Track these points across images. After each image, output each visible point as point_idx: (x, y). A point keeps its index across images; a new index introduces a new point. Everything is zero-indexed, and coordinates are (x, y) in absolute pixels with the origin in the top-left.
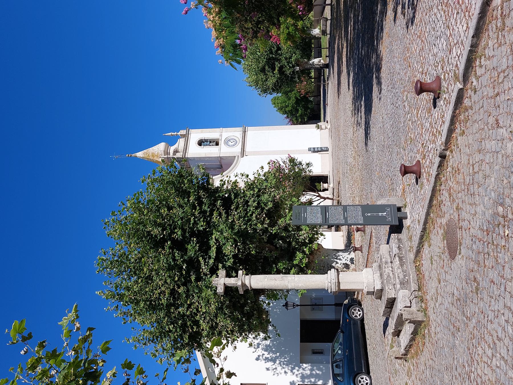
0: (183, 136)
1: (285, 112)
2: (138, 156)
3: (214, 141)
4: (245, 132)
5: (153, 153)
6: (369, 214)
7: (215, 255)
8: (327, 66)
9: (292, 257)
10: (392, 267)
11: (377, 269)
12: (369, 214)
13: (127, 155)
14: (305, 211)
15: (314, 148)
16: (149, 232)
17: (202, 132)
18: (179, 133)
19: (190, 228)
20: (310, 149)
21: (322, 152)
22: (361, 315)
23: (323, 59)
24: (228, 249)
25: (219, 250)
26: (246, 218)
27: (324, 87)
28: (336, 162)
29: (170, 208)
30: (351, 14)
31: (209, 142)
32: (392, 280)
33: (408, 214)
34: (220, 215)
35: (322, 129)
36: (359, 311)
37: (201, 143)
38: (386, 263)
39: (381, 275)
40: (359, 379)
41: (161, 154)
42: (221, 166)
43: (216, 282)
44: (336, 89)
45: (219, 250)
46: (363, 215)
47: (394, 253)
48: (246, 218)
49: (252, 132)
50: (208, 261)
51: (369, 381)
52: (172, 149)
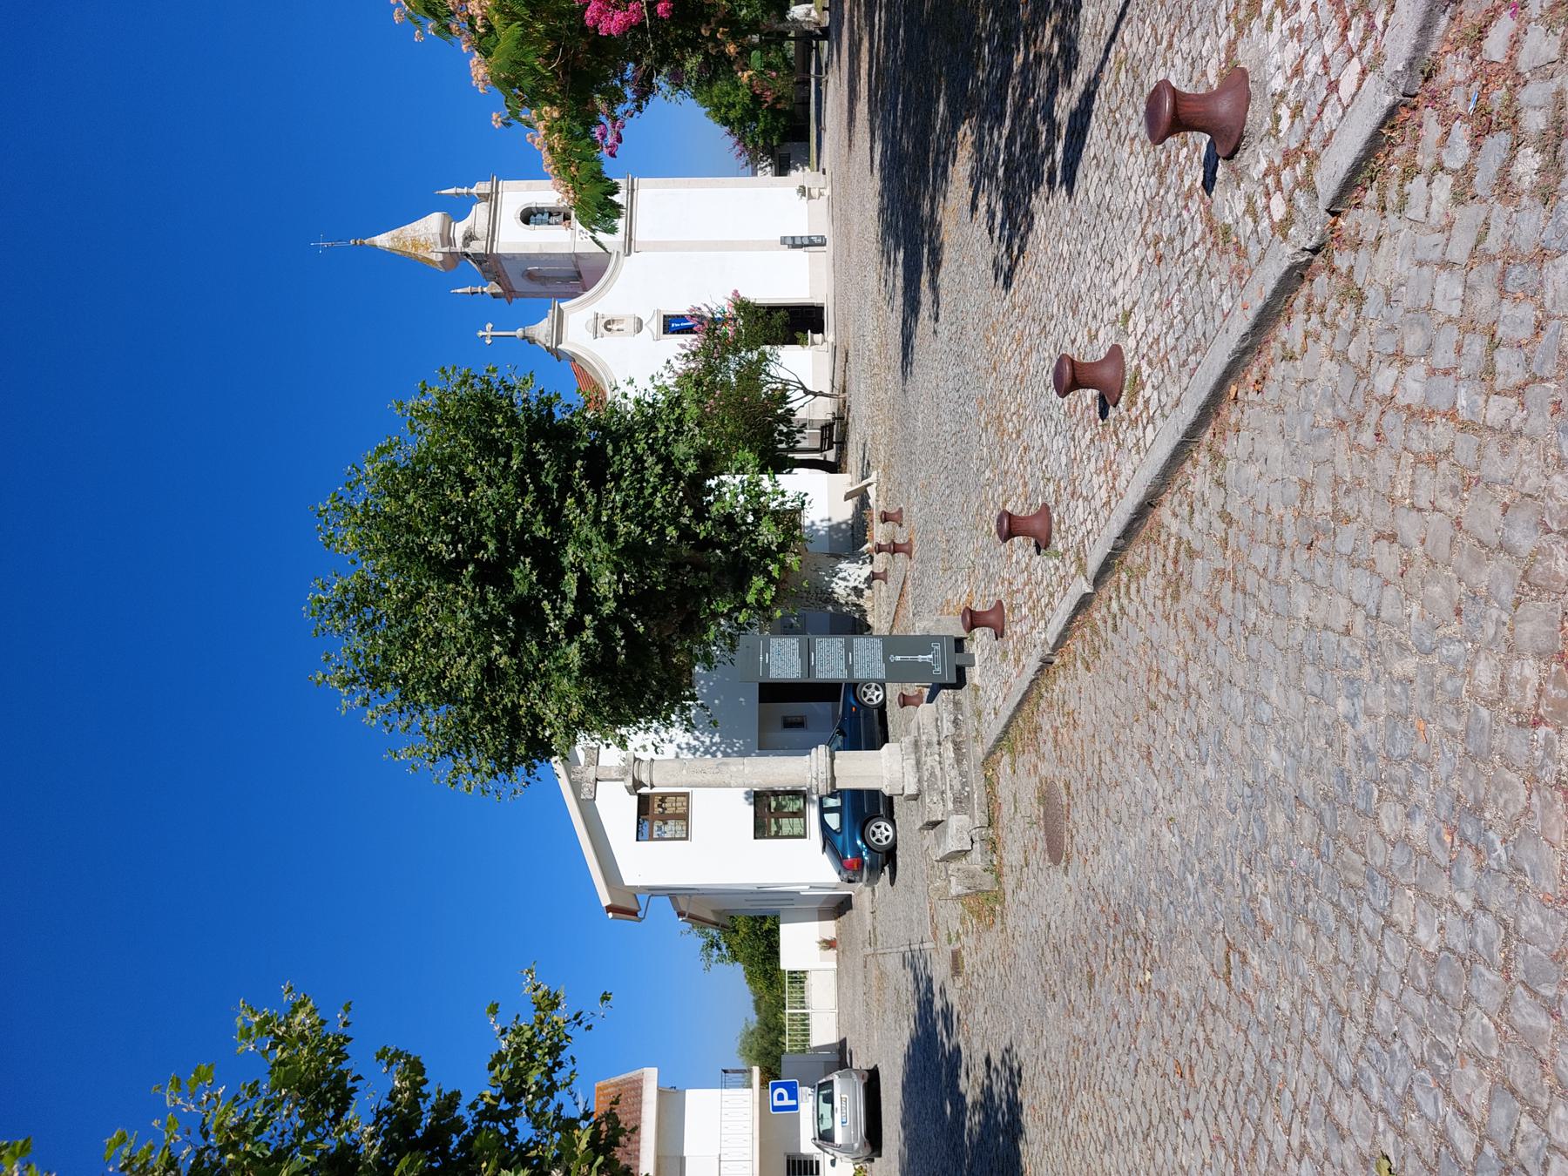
0: (484, 197)
1: (725, 121)
2: (378, 244)
3: (559, 214)
4: (633, 190)
5: (414, 240)
6: (898, 658)
7: (575, 593)
8: (825, 33)
9: (741, 585)
10: (940, 755)
11: (910, 750)
12: (898, 658)
13: (352, 242)
14: (767, 650)
15: (793, 238)
16: (423, 548)
17: (529, 189)
18: (474, 191)
19: (515, 531)
20: (783, 241)
21: (811, 248)
22: (881, 697)
23: (816, 9)
24: (605, 582)
25: (585, 582)
26: (641, 502)
27: (818, 84)
28: (840, 267)
29: (468, 485)
30: (879, 49)
31: (546, 215)
32: (939, 783)
33: (976, 659)
34: (580, 501)
35: (810, 197)
36: (877, 689)
37: (527, 217)
38: (929, 744)
39: (918, 763)
40: (873, 828)
41: (435, 243)
42: (579, 273)
43: (579, 776)
44: (845, 123)
45: (585, 582)
46: (886, 659)
47: (945, 733)
48: (641, 502)
49: (505, 185)
50: (562, 607)
51: (890, 833)
52: (459, 230)
